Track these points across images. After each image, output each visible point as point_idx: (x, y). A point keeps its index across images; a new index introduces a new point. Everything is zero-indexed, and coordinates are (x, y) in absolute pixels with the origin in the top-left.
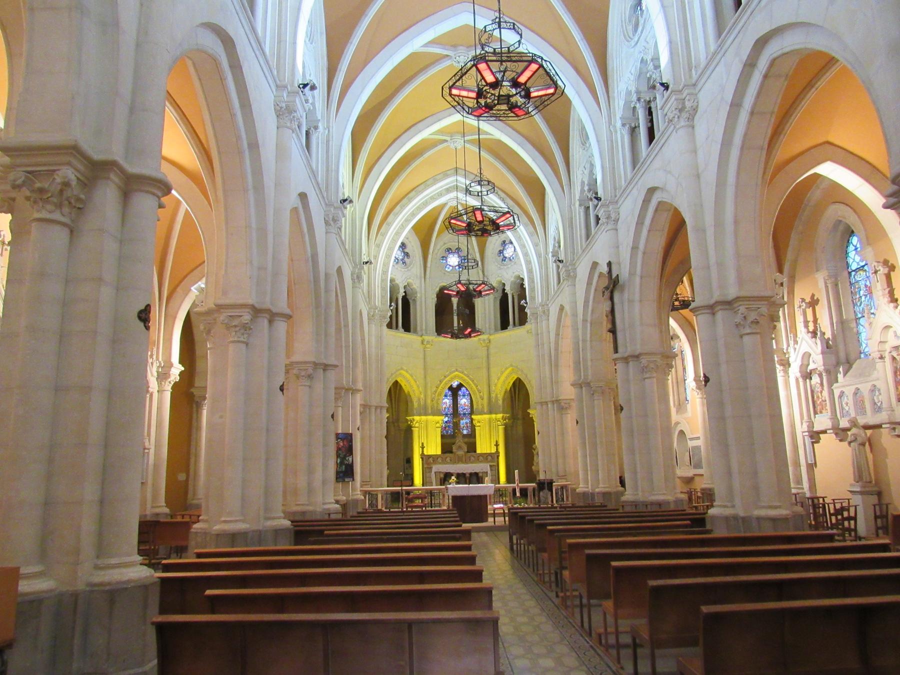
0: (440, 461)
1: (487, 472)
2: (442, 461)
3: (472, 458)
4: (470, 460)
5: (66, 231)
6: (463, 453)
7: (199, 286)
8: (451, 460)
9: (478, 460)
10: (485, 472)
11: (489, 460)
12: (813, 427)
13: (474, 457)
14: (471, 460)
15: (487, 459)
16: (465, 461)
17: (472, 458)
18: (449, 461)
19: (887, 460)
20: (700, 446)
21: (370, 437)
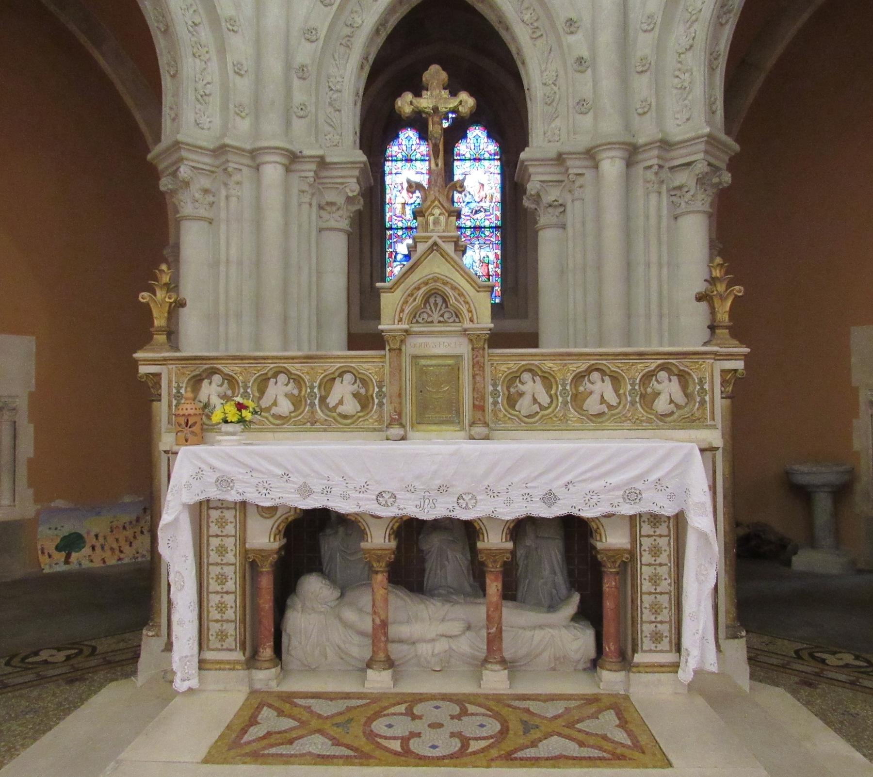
0: (285, 407)
1: (679, 521)
2: (297, 402)
3: (531, 387)
4: (512, 401)
5: (657, 194)
6: (461, 347)
7: (452, 118)
8: (364, 402)
9: (578, 399)
10: (655, 519)
11: (661, 405)
12: (401, 743)
13: (547, 380)
14: (524, 405)
15: (648, 399)
16: (479, 407)
17: (531, 387)
18: (351, 406)
19: (33, 390)
20: (727, 638)
21: (228, 261)
